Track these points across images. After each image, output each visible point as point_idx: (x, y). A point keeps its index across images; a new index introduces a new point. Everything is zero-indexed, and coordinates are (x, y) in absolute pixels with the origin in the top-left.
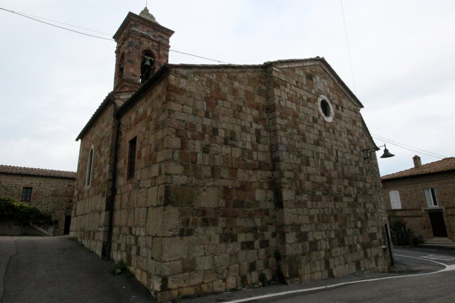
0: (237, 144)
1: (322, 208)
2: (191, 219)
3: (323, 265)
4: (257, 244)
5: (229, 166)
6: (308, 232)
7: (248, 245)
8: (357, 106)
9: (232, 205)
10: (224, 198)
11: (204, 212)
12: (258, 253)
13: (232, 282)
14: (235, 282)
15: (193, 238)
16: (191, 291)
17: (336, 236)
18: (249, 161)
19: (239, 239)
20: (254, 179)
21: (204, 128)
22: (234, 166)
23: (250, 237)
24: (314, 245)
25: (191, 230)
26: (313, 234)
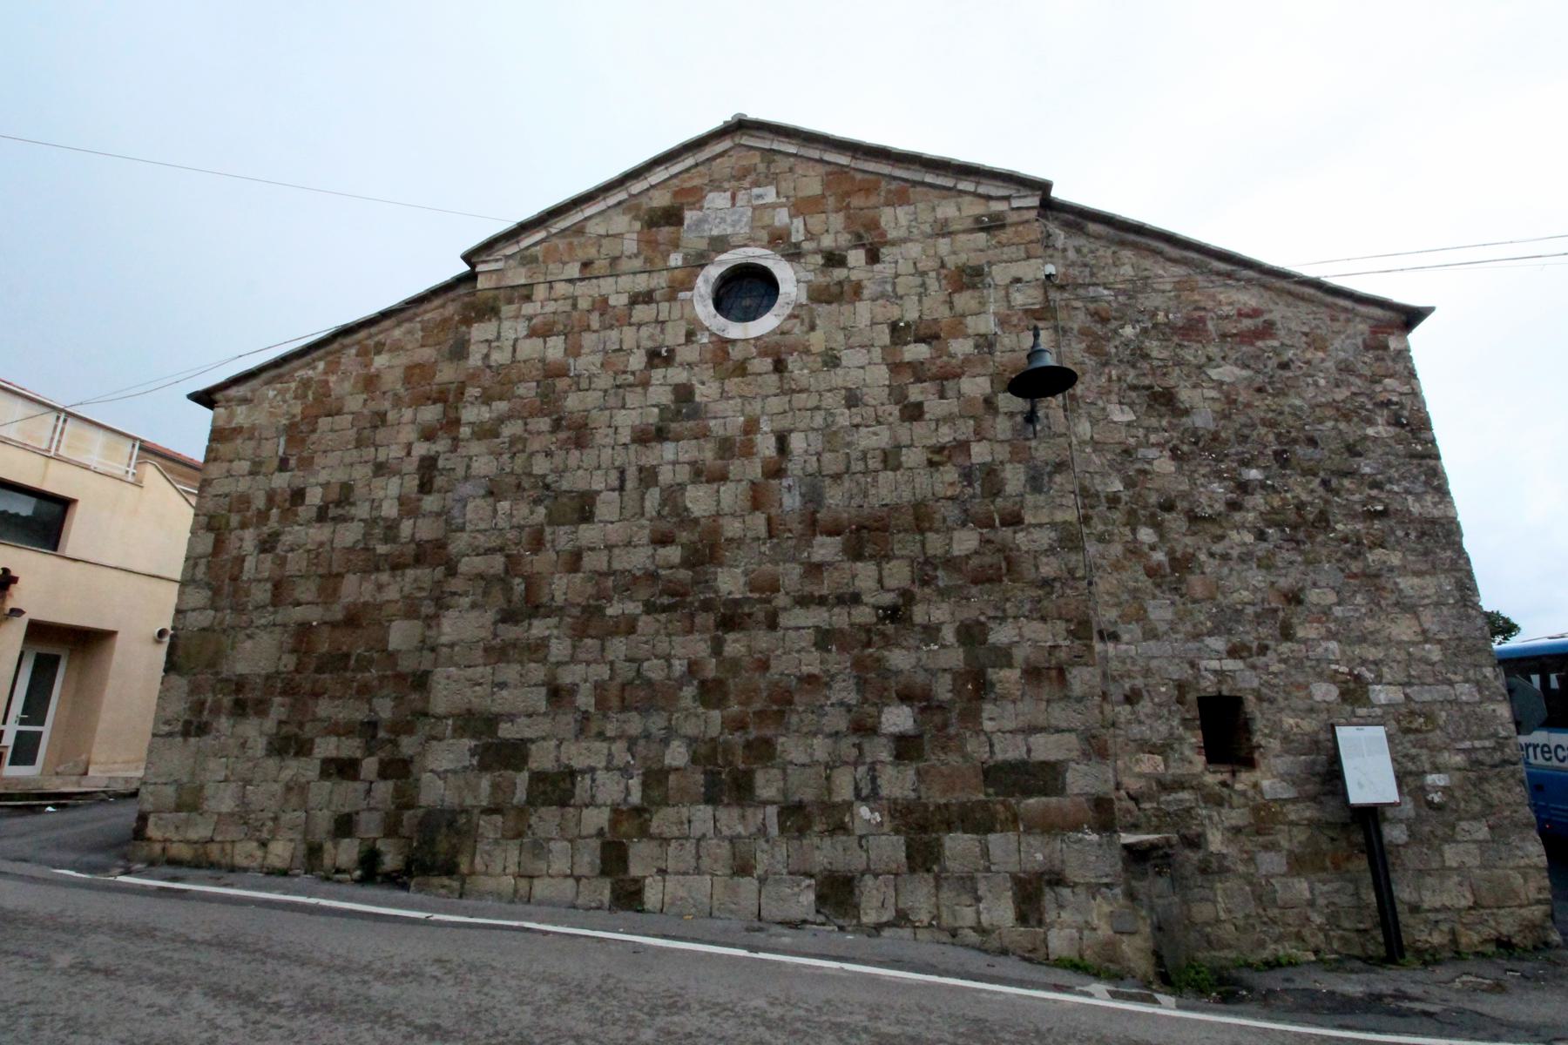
0: (353, 511)
1: (629, 660)
2: (210, 700)
3: (589, 858)
4: (370, 766)
5: (321, 571)
6: (532, 741)
7: (343, 769)
8: (1007, 198)
9: (312, 667)
10: (293, 651)
11: (240, 684)
12: (369, 791)
13: (280, 852)
14: (287, 855)
15: (208, 741)
16: (185, 852)
17: (694, 760)
18: (382, 549)
19: (316, 751)
20: (392, 593)
21: (271, 498)
22: (335, 570)
23: (349, 747)
24: (557, 788)
25: (206, 723)
26: (558, 746)
